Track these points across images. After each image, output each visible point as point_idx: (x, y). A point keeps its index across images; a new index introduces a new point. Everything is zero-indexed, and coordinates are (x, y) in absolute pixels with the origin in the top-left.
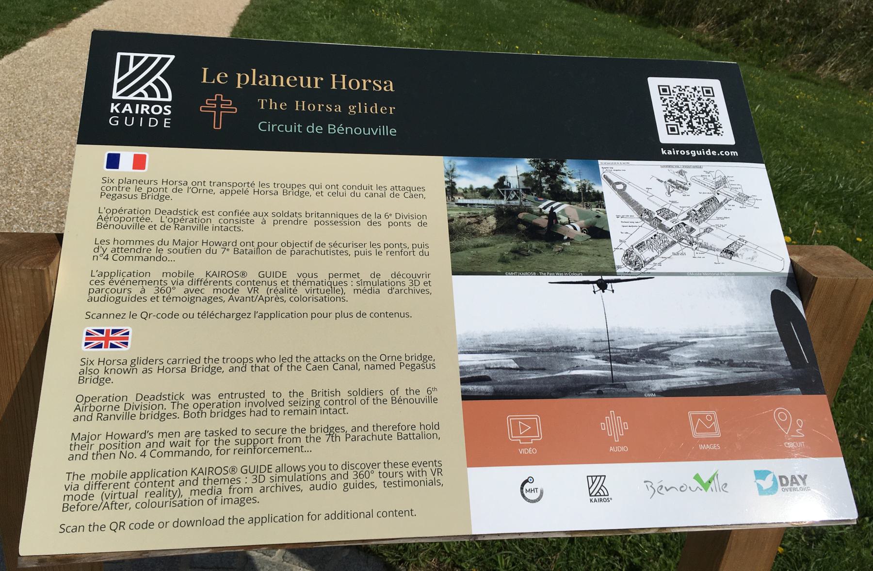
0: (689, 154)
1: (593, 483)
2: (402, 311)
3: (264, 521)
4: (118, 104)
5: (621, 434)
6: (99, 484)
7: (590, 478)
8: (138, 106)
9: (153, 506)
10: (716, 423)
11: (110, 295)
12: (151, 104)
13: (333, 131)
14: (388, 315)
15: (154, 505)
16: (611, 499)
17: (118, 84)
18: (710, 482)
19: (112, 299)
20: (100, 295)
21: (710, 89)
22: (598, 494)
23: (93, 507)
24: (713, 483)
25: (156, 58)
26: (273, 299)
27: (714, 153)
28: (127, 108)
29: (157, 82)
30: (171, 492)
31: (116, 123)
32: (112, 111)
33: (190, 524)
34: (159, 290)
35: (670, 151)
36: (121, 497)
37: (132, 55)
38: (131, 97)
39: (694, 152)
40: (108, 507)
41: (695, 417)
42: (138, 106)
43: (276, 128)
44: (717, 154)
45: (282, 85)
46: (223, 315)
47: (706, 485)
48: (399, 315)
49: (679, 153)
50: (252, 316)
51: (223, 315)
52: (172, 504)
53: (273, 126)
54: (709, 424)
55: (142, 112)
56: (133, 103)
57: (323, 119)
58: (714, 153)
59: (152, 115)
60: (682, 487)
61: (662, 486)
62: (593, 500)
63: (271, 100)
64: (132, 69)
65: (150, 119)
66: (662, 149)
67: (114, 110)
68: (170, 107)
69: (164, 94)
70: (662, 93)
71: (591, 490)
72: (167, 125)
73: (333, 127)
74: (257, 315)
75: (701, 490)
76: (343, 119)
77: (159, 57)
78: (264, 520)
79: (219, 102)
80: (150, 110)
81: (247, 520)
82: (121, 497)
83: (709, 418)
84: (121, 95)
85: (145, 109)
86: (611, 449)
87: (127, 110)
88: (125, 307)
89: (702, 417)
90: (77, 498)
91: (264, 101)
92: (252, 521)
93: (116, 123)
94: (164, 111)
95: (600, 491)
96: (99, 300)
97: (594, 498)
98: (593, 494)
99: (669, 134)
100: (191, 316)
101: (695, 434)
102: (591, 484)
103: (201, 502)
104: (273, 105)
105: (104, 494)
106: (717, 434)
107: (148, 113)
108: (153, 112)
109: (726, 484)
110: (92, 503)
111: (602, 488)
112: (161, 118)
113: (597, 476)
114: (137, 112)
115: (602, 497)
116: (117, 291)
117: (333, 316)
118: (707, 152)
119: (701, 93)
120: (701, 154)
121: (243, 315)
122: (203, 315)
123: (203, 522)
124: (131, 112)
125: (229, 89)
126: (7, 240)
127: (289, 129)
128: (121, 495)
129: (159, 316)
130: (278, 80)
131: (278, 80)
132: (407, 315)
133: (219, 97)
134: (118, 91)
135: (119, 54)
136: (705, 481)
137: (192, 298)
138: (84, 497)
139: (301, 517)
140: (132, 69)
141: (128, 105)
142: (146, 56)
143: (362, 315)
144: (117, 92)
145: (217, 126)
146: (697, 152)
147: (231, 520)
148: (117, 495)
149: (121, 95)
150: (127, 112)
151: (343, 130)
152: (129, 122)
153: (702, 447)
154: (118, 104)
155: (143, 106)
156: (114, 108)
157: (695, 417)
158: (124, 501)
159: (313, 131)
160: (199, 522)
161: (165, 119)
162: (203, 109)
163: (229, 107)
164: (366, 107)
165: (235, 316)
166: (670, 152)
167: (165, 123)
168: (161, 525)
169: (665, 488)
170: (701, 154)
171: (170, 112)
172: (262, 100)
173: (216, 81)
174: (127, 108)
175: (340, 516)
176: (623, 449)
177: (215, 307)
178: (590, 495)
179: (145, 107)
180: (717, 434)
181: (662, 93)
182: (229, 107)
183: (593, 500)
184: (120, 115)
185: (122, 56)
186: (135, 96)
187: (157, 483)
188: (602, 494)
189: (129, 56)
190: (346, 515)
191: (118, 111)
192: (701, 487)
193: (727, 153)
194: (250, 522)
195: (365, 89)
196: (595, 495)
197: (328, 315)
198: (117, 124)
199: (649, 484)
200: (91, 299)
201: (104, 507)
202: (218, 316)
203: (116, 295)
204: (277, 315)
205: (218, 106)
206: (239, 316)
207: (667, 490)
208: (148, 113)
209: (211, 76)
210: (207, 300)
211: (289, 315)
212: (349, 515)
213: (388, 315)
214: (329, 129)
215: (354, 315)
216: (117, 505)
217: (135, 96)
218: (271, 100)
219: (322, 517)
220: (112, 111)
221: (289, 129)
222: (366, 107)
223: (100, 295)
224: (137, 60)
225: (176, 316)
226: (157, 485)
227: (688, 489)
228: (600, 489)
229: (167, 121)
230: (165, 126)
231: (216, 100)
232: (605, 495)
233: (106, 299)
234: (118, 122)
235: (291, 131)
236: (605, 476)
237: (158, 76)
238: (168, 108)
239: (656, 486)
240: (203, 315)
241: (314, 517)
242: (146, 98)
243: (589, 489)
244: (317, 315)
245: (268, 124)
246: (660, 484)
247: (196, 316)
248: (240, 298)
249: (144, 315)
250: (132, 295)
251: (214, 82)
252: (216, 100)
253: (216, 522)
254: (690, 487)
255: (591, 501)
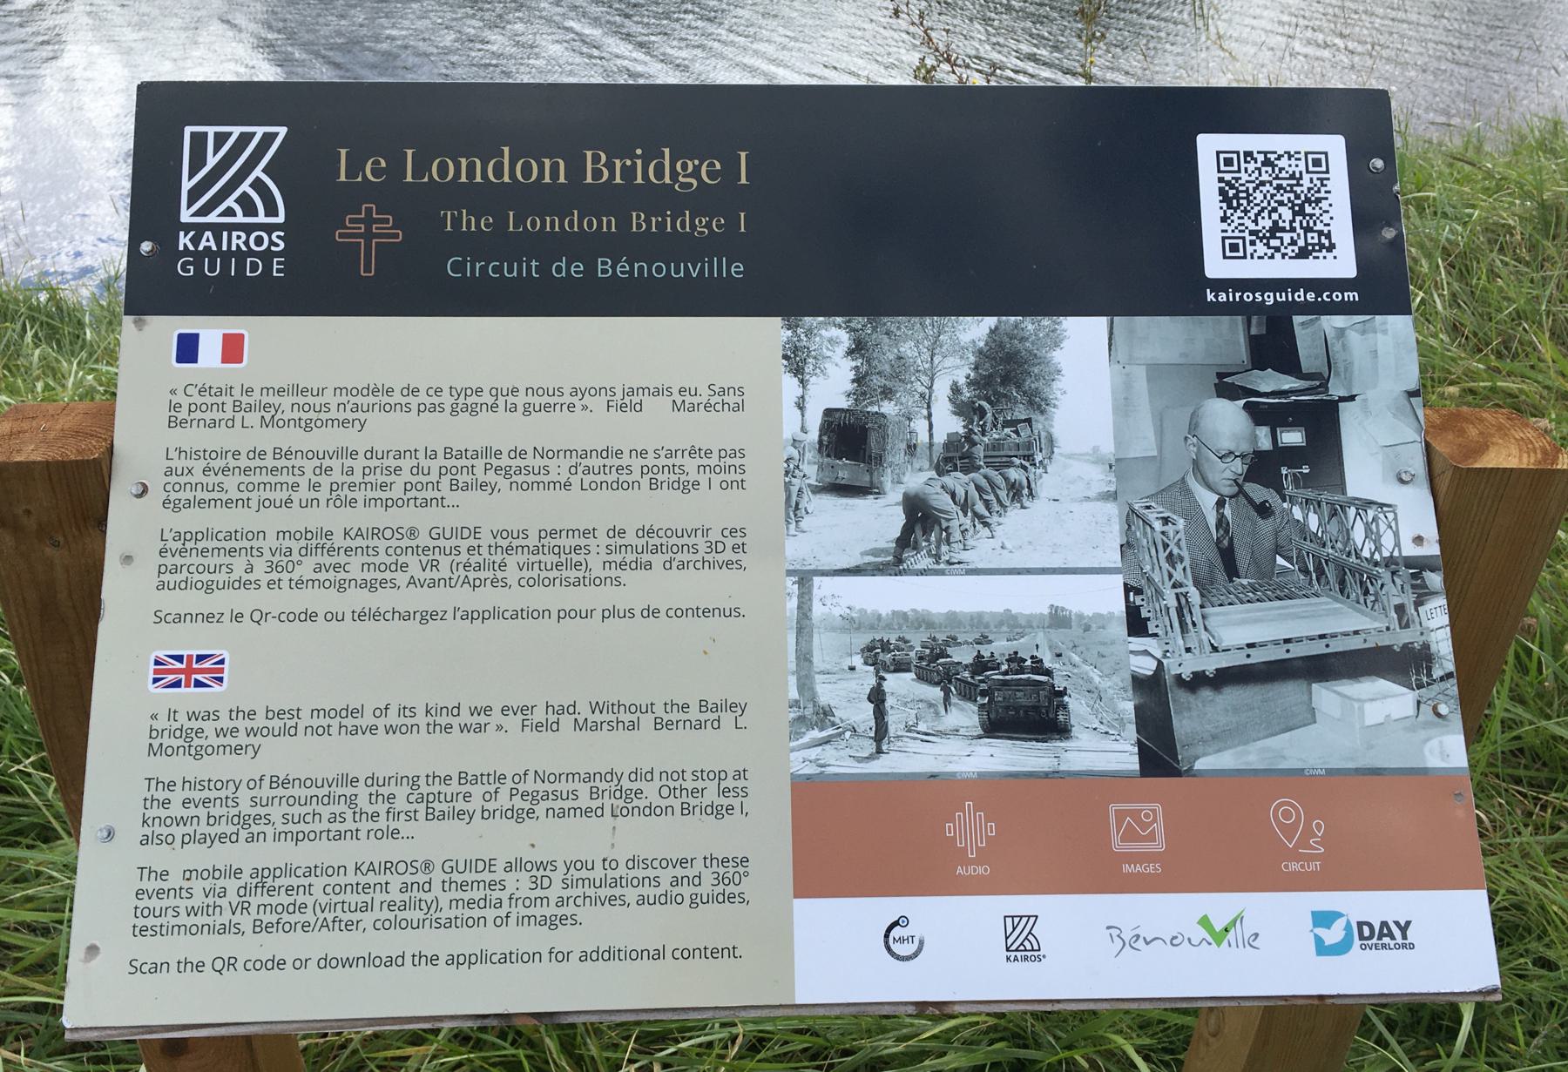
0: (1261, 299)
1: (1014, 929)
2: (727, 605)
3: (473, 960)
4: (192, 233)
5: (982, 843)
6: (263, 887)
7: (1009, 920)
8: (225, 234)
9: (403, 925)
10: (1159, 827)
11: (196, 577)
12: (248, 229)
13: (607, 271)
14: (700, 612)
15: (404, 924)
16: (1044, 956)
17: (189, 191)
18: (1226, 930)
19: (199, 585)
20: (179, 577)
21: (1323, 157)
22: (1022, 948)
23: (303, 926)
24: (1232, 931)
25: (254, 134)
26: (488, 582)
27: (1311, 296)
28: (208, 240)
29: (258, 185)
30: (423, 903)
31: (189, 271)
32: (181, 248)
33: (348, 963)
34: (274, 566)
35: (1224, 295)
36: (346, 909)
37: (211, 130)
38: (213, 218)
39: (1272, 294)
40: (327, 926)
41: (1121, 815)
42: (225, 234)
43: (484, 269)
44: (1316, 298)
45: (478, 179)
46: (397, 615)
47: (1219, 936)
48: (722, 613)
49: (1241, 297)
50: (449, 615)
51: (397, 615)
52: (434, 924)
53: (478, 265)
54: (1144, 826)
55: (234, 248)
56: (217, 229)
57: (585, 247)
58: (1311, 296)
59: (251, 253)
60: (1175, 938)
61: (1138, 936)
62: (1012, 959)
63: (464, 211)
64: (212, 161)
65: (249, 260)
66: (1208, 290)
67: (185, 245)
68: (282, 234)
69: (271, 210)
70: (1223, 168)
71: (1010, 941)
72: (279, 271)
73: (606, 263)
74: (459, 614)
75: (1210, 944)
76: (623, 244)
77: (260, 131)
78: (473, 959)
79: (369, 221)
80: (246, 243)
81: (443, 959)
82: (346, 909)
83: (1147, 816)
84: (194, 215)
85: (238, 240)
86: (959, 870)
87: (208, 244)
88: (221, 601)
89: (1135, 814)
90: (280, 909)
91: (452, 215)
92: (452, 960)
93: (189, 271)
94: (272, 243)
95: (1026, 943)
96: (177, 586)
97: (1013, 954)
98: (1013, 948)
99: (1225, 257)
100: (340, 618)
101: (1118, 845)
102: (1010, 930)
103: (482, 920)
104: (469, 222)
105: (317, 905)
106: (1159, 845)
107: (244, 248)
108: (253, 247)
109: (1256, 935)
110: (303, 918)
111: (1030, 937)
112: (267, 256)
113: (1021, 917)
114: (225, 248)
115: (1029, 954)
116: (207, 569)
117: (597, 615)
118: (1297, 294)
119: (1302, 164)
120: (1284, 299)
121: (434, 614)
122: (360, 616)
123: (370, 961)
124: (214, 248)
125: (390, 194)
126: (875, 409)
127: (510, 271)
128: (346, 906)
129: (283, 617)
130: (471, 168)
131: (471, 168)
132: (735, 613)
133: (369, 210)
134: (189, 206)
135: (188, 130)
136: (1218, 928)
137: (342, 582)
138: (291, 909)
139: (537, 956)
140: (212, 161)
141: (208, 234)
142: (236, 131)
143: (653, 613)
144: (188, 208)
145: (367, 270)
146: (1278, 294)
147: (182, 965)
148: (339, 906)
149: (194, 215)
150: (207, 248)
151: (628, 269)
152: (212, 269)
153: (1127, 868)
154: (192, 233)
155: (235, 234)
156: (184, 240)
157: (1121, 815)
158: (355, 917)
159: (564, 274)
160: (361, 960)
161: (275, 260)
162: (341, 236)
163: (388, 230)
164: (669, 219)
165: (418, 616)
166: (1223, 297)
167: (275, 267)
168: (298, 964)
169: (1144, 938)
170: (1284, 299)
171: (282, 245)
172: (449, 213)
173: (364, 176)
174: (208, 240)
175: (606, 956)
176: (980, 870)
177: (382, 600)
178: (1008, 950)
179: (239, 237)
180: (1159, 845)
181: (1223, 168)
182: (388, 230)
183: (1012, 959)
184: (195, 254)
185: (192, 134)
186: (219, 215)
187: (360, 887)
188: (1029, 947)
189: (206, 134)
190: (617, 953)
191: (191, 248)
192: (1210, 940)
193: (1337, 297)
194: (450, 962)
195: (618, 180)
196: (1017, 950)
197: (589, 614)
198: (192, 273)
199: (1115, 932)
200: (162, 586)
201: (322, 926)
202: (389, 616)
203: (206, 577)
204: (497, 614)
205: (369, 229)
206: (428, 617)
207: (1147, 943)
208: (244, 248)
209: (355, 167)
210: (369, 585)
211: (516, 615)
212: (622, 954)
213: (700, 612)
214: (600, 267)
215: (637, 612)
216: (343, 924)
217: (219, 215)
218: (464, 211)
219: (574, 957)
220: (181, 248)
221: (510, 271)
222: (669, 219)
223: (179, 577)
224: (221, 139)
225: (312, 616)
226: (360, 890)
227: (1186, 940)
228: (1026, 938)
229: (278, 263)
230: (275, 274)
231: (363, 216)
232: (1033, 950)
233: (187, 585)
234: (192, 268)
235: (515, 274)
236: (1037, 917)
237: (258, 172)
238: (278, 237)
239: (1127, 936)
240: (360, 616)
241: (560, 957)
242: (240, 218)
243: (1007, 938)
244: (567, 614)
245: (465, 261)
246: (1136, 932)
247: (348, 616)
248: (427, 582)
249: (257, 616)
250: (234, 576)
251: (360, 179)
252: (363, 216)
253: (390, 962)
254: (1189, 939)
255: (1008, 959)
